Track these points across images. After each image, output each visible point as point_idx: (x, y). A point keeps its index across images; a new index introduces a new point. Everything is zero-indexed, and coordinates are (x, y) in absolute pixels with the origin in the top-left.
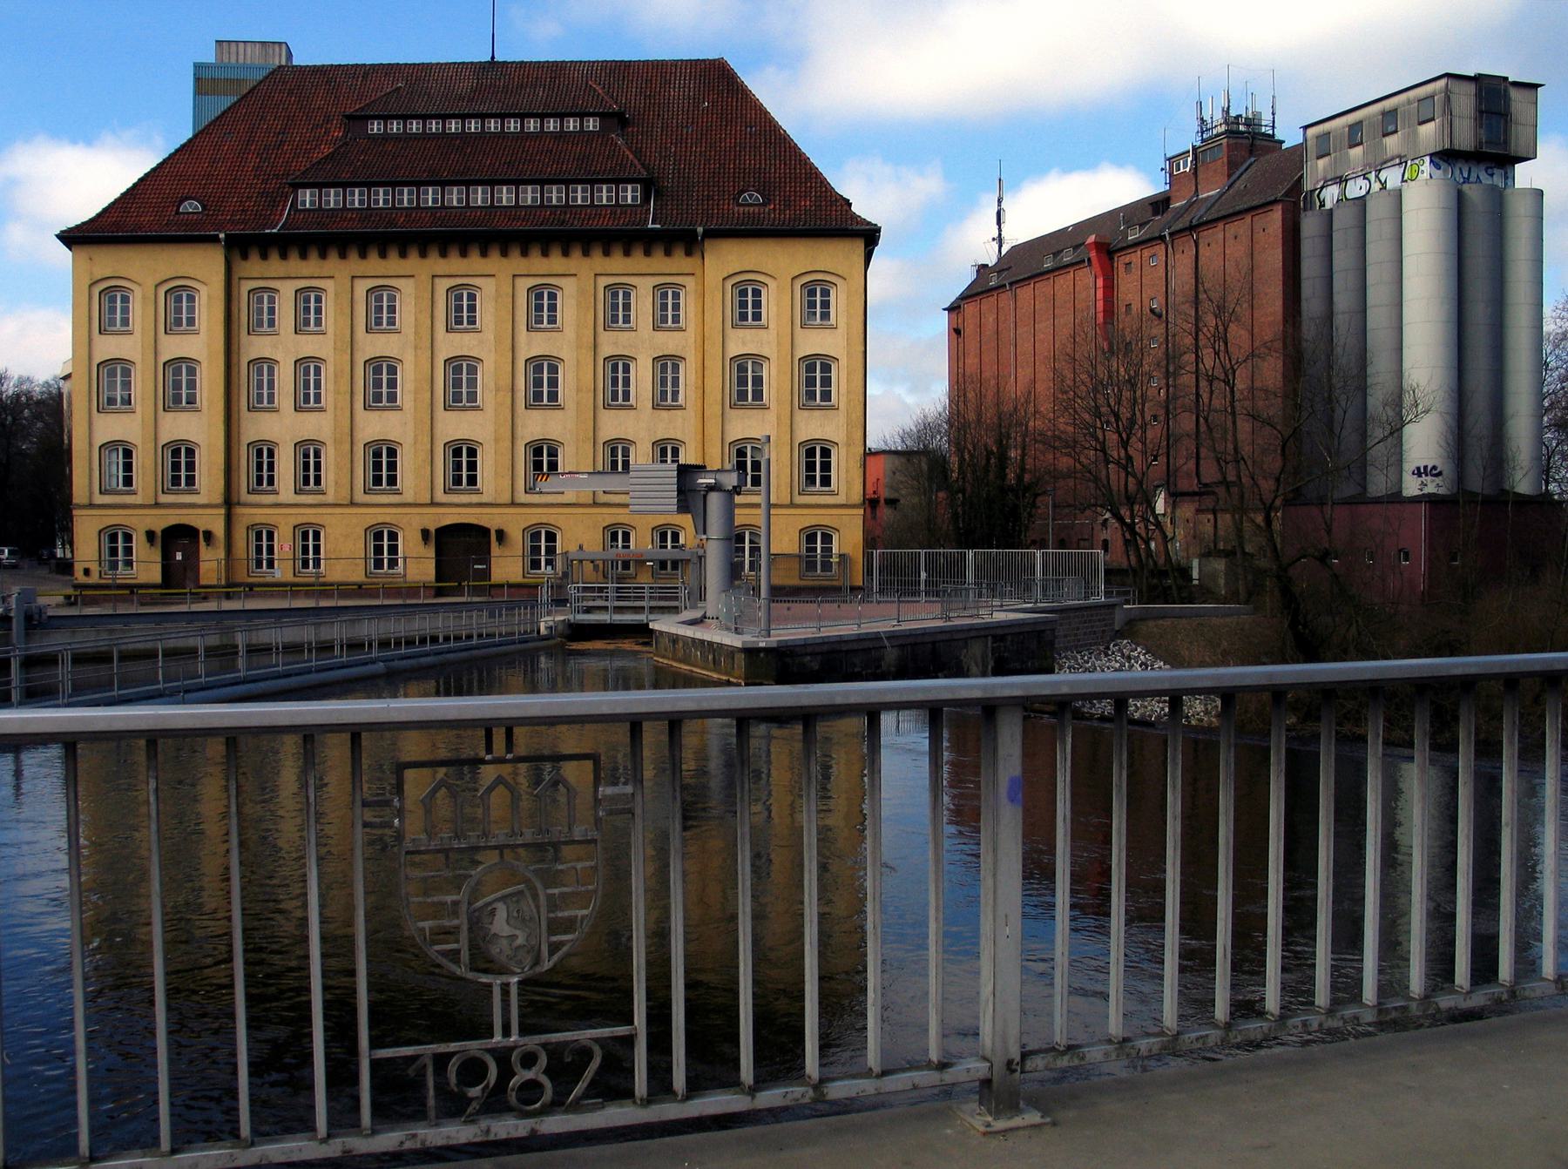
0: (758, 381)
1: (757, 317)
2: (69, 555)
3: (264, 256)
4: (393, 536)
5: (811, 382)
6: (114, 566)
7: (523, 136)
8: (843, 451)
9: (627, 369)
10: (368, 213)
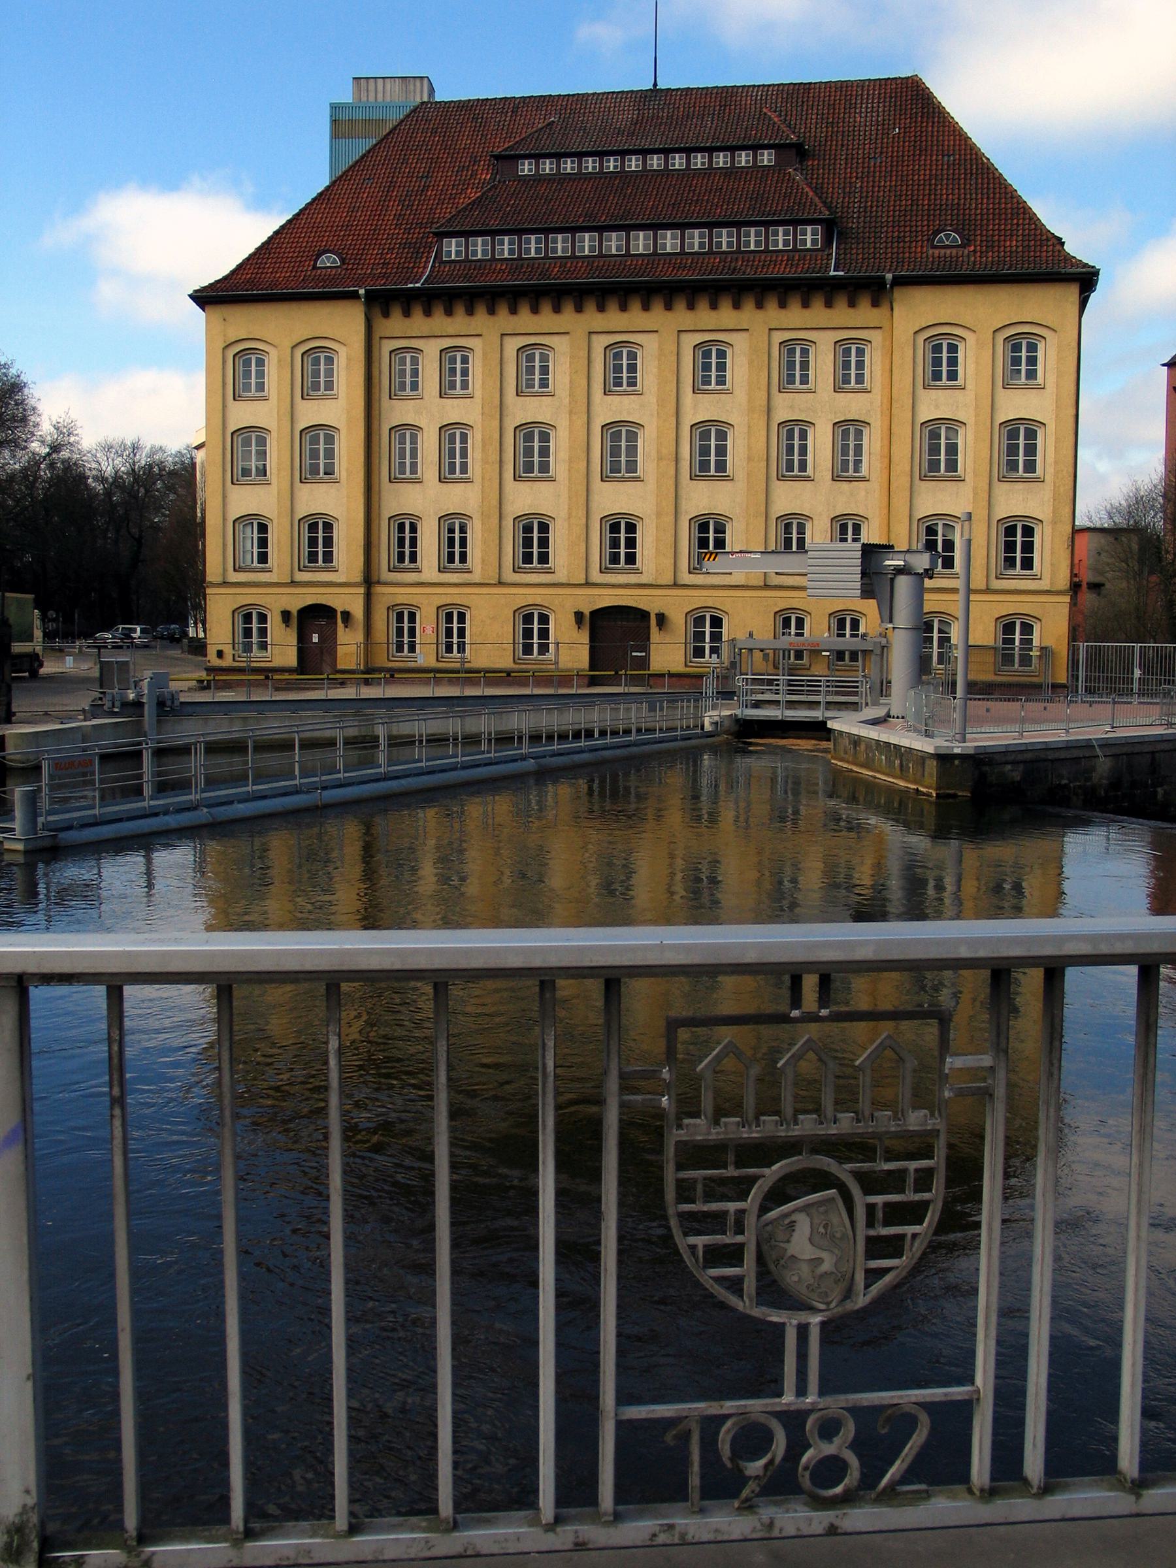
0: (952, 449)
1: (953, 376)
2: (201, 635)
3: (407, 314)
4: (544, 619)
5: (1013, 450)
6: (248, 648)
7: (688, 172)
8: (1048, 529)
9: (803, 436)
10: (518, 263)
